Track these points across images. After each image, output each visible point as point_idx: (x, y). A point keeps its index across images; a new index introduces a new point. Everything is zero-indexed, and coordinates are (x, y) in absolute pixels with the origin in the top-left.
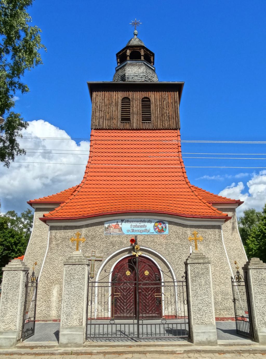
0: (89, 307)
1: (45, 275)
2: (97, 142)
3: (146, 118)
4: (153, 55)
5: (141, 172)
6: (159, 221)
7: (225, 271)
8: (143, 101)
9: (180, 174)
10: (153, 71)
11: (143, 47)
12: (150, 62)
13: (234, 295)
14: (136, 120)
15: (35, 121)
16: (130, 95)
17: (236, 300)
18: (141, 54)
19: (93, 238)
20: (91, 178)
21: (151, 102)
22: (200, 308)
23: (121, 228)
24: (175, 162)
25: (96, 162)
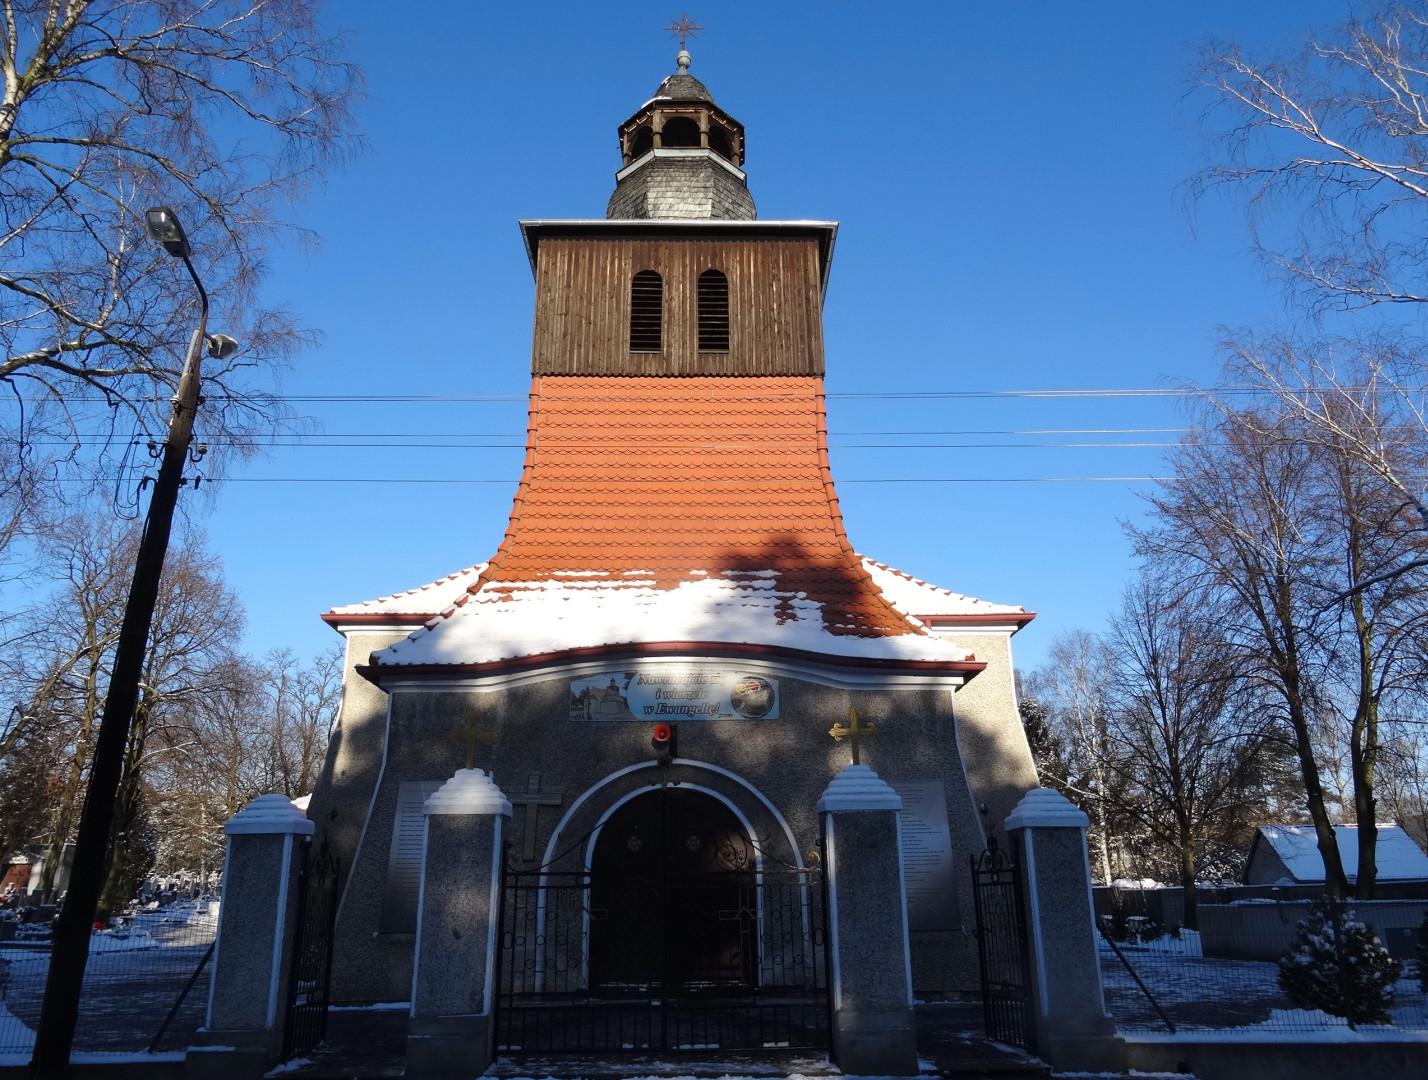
0: (506, 953)
1: (374, 853)
2: (553, 418)
3: (713, 335)
4: (741, 129)
5: (693, 517)
6: (750, 678)
7: (961, 841)
9: (821, 524)
10: (738, 185)
13: (979, 917)
17: (985, 932)
18: (699, 128)
20: (530, 537)
21: (730, 286)
22: (864, 956)
23: (625, 699)
24: (807, 485)
25: (546, 484)
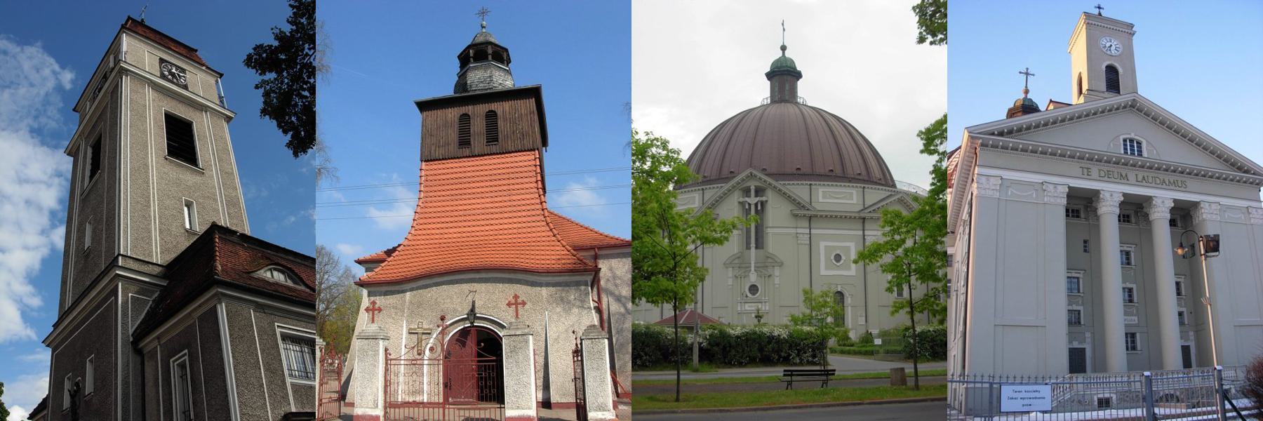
11: (491, 43)
12: (502, 61)
14: (478, 142)
16: (469, 109)
19: (420, 305)
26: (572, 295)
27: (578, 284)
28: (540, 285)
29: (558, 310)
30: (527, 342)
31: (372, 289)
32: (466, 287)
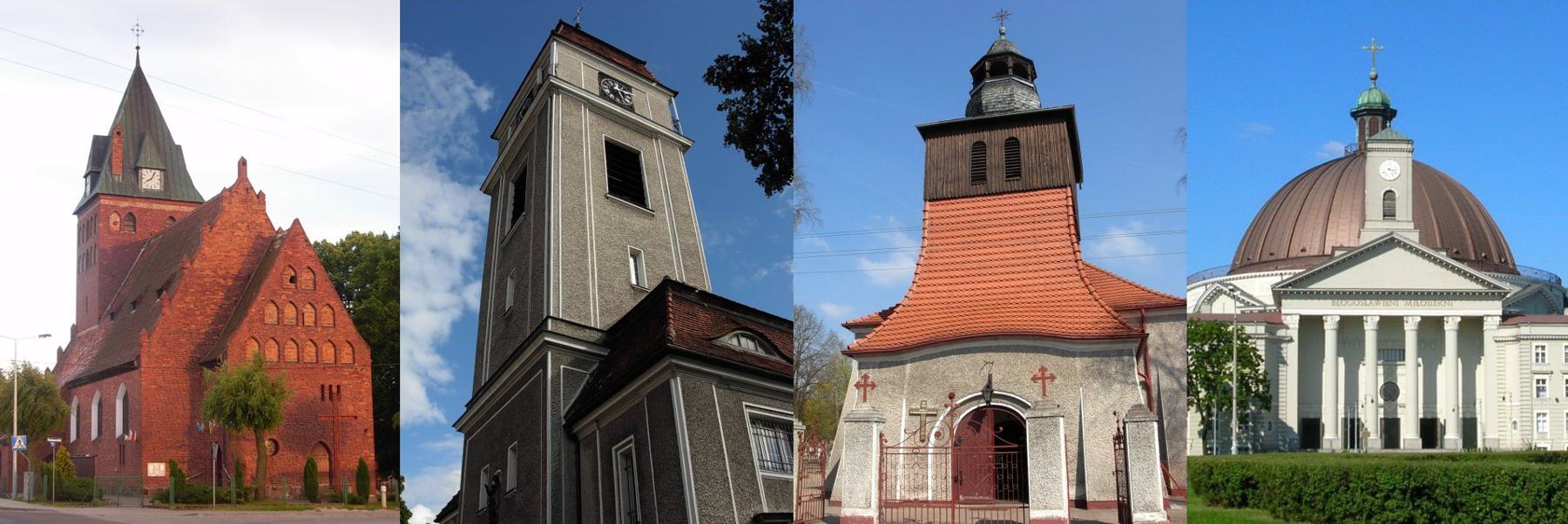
8: (1007, 144)
11: (1012, 54)
14: (996, 177)
15: (73, 321)
16: (985, 136)
26: (1113, 367)
27: (1120, 353)
28: (1073, 355)
29: (1095, 385)
30: (1057, 425)
31: (865, 360)
32: (980, 357)
